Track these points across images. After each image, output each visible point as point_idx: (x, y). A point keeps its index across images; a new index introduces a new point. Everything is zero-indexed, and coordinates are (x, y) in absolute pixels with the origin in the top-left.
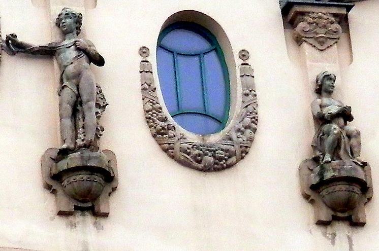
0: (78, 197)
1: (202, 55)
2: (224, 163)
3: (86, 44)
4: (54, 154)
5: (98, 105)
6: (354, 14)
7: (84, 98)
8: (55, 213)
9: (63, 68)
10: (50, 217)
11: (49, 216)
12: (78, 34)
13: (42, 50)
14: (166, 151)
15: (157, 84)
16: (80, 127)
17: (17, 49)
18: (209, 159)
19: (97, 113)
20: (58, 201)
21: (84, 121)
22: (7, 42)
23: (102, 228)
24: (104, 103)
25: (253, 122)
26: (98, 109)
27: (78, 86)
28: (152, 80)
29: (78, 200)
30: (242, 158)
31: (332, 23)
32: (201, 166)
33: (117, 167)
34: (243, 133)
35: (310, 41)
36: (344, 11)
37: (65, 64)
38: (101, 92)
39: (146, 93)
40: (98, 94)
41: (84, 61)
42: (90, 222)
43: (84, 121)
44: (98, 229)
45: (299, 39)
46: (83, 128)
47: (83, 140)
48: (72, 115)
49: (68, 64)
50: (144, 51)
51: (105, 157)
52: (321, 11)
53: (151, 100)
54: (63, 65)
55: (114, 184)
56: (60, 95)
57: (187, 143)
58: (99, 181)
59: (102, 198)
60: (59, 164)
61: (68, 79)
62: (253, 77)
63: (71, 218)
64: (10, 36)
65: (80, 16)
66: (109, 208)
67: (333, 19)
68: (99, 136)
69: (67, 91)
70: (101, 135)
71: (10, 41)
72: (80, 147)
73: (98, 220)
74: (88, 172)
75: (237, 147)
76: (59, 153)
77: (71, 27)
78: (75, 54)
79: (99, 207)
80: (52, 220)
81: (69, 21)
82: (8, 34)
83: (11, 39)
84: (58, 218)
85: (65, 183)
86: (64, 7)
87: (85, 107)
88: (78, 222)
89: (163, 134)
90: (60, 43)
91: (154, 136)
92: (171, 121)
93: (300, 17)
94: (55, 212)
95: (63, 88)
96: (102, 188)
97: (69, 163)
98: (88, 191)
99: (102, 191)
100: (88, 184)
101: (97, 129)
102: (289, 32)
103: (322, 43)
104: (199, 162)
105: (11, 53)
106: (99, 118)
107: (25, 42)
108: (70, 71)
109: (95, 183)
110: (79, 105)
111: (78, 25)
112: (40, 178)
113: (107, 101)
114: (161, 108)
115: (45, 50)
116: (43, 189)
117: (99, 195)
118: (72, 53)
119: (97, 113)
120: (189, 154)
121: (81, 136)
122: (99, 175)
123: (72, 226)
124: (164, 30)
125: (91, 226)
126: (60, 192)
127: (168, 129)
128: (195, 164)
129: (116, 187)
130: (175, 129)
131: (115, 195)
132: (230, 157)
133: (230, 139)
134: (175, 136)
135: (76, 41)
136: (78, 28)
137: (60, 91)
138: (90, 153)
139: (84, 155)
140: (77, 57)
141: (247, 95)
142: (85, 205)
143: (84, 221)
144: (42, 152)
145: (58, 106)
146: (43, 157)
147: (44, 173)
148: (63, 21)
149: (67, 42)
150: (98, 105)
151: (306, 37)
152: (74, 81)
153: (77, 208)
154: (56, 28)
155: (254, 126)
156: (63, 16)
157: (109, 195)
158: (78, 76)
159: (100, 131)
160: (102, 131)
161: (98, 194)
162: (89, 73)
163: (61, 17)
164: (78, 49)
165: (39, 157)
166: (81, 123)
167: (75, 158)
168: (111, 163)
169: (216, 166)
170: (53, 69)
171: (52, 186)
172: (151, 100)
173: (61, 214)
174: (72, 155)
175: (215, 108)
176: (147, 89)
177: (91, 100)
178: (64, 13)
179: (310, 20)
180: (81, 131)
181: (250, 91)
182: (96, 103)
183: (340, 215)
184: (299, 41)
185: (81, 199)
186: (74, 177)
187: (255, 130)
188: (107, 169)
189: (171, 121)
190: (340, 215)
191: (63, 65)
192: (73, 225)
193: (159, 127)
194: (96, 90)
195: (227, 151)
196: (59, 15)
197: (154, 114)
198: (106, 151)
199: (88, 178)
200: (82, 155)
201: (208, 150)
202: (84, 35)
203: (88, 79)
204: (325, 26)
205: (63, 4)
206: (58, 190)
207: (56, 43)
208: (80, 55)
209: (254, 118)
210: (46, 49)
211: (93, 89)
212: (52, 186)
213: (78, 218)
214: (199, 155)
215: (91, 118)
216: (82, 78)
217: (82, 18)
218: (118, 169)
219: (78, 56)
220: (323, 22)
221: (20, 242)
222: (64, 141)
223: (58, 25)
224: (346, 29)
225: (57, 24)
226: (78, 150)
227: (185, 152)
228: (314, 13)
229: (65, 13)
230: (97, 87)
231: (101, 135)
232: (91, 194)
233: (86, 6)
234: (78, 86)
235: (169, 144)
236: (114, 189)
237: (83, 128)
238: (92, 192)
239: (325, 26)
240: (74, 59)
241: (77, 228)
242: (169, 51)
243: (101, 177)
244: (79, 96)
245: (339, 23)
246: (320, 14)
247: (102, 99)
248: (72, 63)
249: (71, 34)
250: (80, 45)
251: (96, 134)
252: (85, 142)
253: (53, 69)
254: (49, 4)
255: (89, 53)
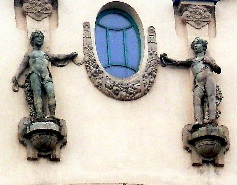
0: (204, 155)
1: (124, 30)
2: (133, 97)
3: (210, 60)
4: (190, 128)
5: (217, 98)
6: (218, 6)
7: (209, 93)
8: (190, 165)
9: (195, 75)
10: (188, 167)
11: (187, 167)
12: (205, 53)
13: (182, 63)
14: (97, 87)
15: (94, 45)
16: (206, 111)
17: (167, 63)
18: (123, 93)
19: (217, 102)
20: (193, 157)
21: (208, 107)
22: (161, 58)
23: (220, 174)
24: (221, 96)
25: (154, 71)
26: (217, 100)
27: (205, 86)
28: (90, 42)
29: (203, 156)
30: (145, 94)
31: (205, 12)
32: (119, 96)
33: (229, 136)
34: (146, 77)
35: (192, 23)
36: (212, 4)
37: (197, 72)
38: (219, 89)
39: (86, 51)
40: (217, 90)
41: (208, 70)
42: (212, 170)
43: (208, 107)
44: (217, 174)
45: (184, 22)
46: (208, 112)
47: (208, 119)
48: (201, 104)
49: (199, 72)
50: (86, 25)
51: (222, 130)
52: (197, 4)
53: (89, 55)
54: (195, 73)
55: (227, 147)
56: (194, 92)
57: (110, 82)
58: (218, 145)
59: (220, 155)
60: (193, 134)
61: (199, 82)
62: (156, 43)
63: (201, 168)
64: (163, 55)
65: (206, 42)
66: (224, 161)
67: (206, 9)
68: (218, 117)
69: (197, 89)
70: (219, 116)
71: (163, 58)
72: (206, 124)
73: (217, 169)
74: (211, 140)
75: (142, 86)
76: (193, 128)
77: (201, 49)
78: (203, 66)
79: (218, 161)
80: (189, 169)
81: (199, 45)
82: (162, 53)
83: (164, 56)
84: (192, 167)
85: (197, 146)
86: (196, 37)
87: (209, 99)
88: (205, 170)
89: (95, 76)
90: (194, 59)
91: (90, 77)
92: (103, 69)
93: (185, 8)
94: (191, 164)
95: (196, 87)
96: (219, 149)
97: (199, 134)
98: (211, 151)
99: (219, 151)
100: (211, 147)
101: (217, 113)
102: (178, 18)
103: (198, 24)
104: (117, 94)
105: (163, 65)
106: (217, 105)
107: (172, 58)
108: (200, 76)
109: (215, 146)
110: (205, 98)
111: (205, 48)
112: (182, 143)
113: (223, 95)
114: (95, 60)
115: (184, 63)
116: (183, 149)
117: (218, 154)
118: (201, 65)
119: (217, 102)
120: (110, 89)
121: (207, 117)
122: (218, 141)
123: (201, 172)
124: (100, 14)
125: (213, 172)
126: (194, 151)
127: (99, 73)
128: (115, 96)
129: (228, 149)
130: (103, 73)
131: (228, 153)
132: (137, 93)
133: (139, 82)
134: (102, 77)
135: (203, 58)
136: (205, 50)
137: (194, 89)
138: (212, 127)
139: (209, 129)
140: (204, 68)
141: (151, 54)
142: (209, 160)
143: (208, 170)
144: (183, 127)
145: (192, 98)
146: (183, 130)
147: (183, 140)
148: (196, 45)
149: (198, 59)
150: (217, 98)
151: (188, 21)
152: (202, 83)
153: (204, 162)
154: (191, 51)
155: (154, 73)
156: (195, 42)
157: (224, 154)
158: (205, 79)
159: (219, 114)
160: (220, 114)
161: (217, 153)
162: (212, 78)
163: (194, 43)
164: (205, 63)
165: (181, 130)
166: (206, 109)
167: (203, 130)
168: (225, 133)
169: (127, 98)
170: (189, 75)
171: (188, 148)
172: (89, 55)
173: (194, 165)
174: (201, 129)
175: (132, 63)
176: (86, 48)
177: (213, 95)
178: (196, 40)
179: (191, 9)
180: (206, 113)
181: (153, 52)
182: (216, 97)
183: (42, 154)
184: (184, 22)
185: (207, 156)
186: (202, 142)
187: (155, 76)
188: (223, 137)
189: (101, 68)
190: (42, 154)
191: (195, 73)
192: (202, 172)
193: (93, 72)
194: (216, 89)
195: (136, 89)
196: (193, 42)
197: (90, 64)
198: (222, 126)
199: (211, 143)
200: (207, 128)
201: (123, 88)
202: (209, 54)
203: (211, 82)
204: (200, 14)
205: (196, 35)
206: (192, 150)
207: (191, 59)
208: (206, 67)
209: (155, 68)
210: (185, 63)
211: (214, 88)
212: (188, 148)
213: (205, 168)
214: (117, 90)
215: (213, 106)
216: (207, 81)
217: (207, 44)
218: (230, 138)
219: (205, 67)
220: (199, 11)
221: (169, 182)
222: (196, 120)
223: (192, 48)
224: (214, 16)
225: (192, 47)
226: (205, 125)
227: (109, 88)
228: (193, 5)
229: (197, 40)
230: (216, 86)
231: (219, 116)
232: (213, 153)
233: (210, 36)
234: (205, 86)
235: (99, 82)
236: (227, 150)
237: (208, 112)
238: (213, 152)
239: (200, 14)
240: (202, 69)
241: (204, 174)
242: (104, 28)
243: (219, 142)
244: (205, 92)
245: (211, 12)
246: (197, 6)
247: (220, 94)
248: (201, 72)
249: (200, 54)
250: (206, 60)
251: (216, 115)
252: (209, 120)
253: (189, 75)
254: (187, 35)
255: (211, 65)
